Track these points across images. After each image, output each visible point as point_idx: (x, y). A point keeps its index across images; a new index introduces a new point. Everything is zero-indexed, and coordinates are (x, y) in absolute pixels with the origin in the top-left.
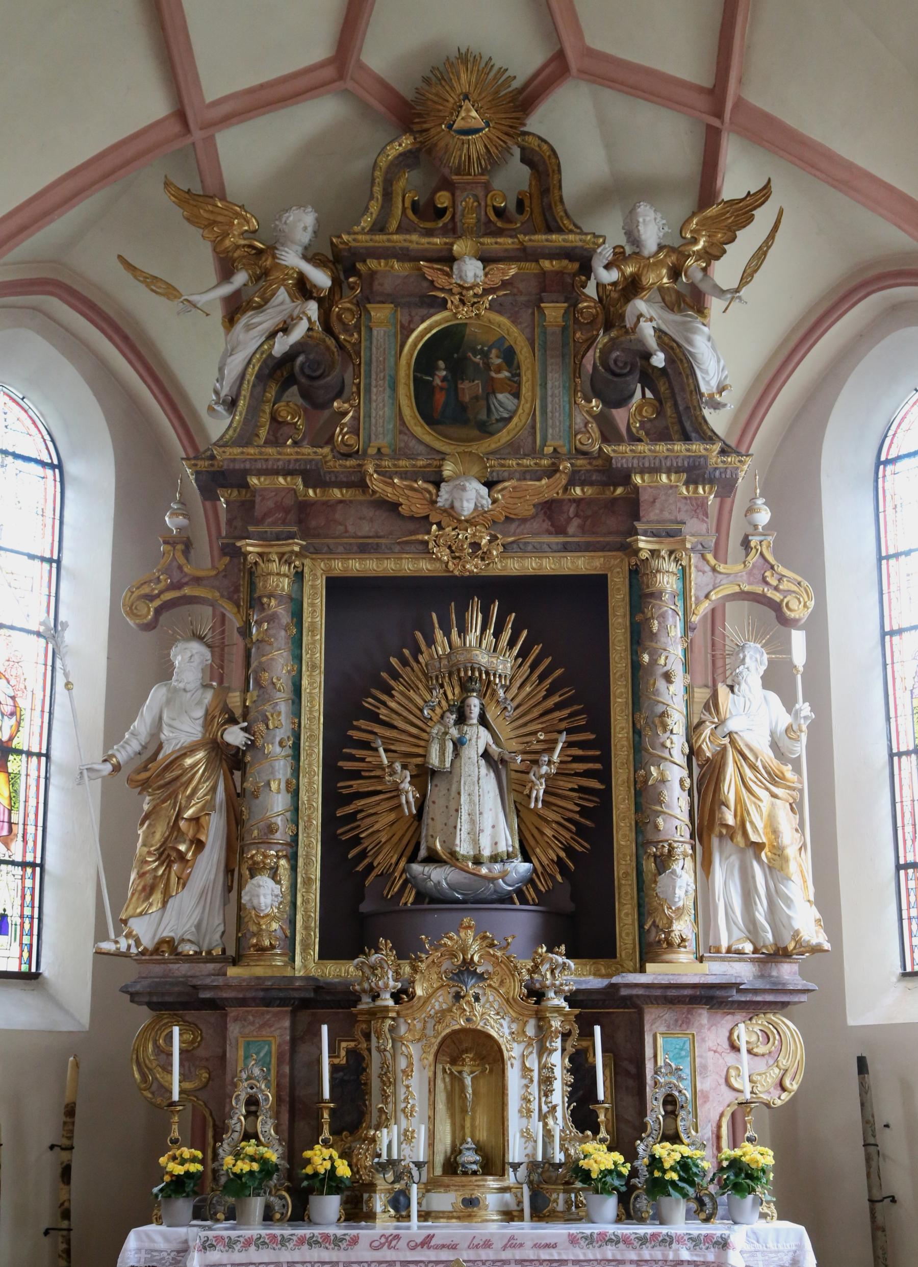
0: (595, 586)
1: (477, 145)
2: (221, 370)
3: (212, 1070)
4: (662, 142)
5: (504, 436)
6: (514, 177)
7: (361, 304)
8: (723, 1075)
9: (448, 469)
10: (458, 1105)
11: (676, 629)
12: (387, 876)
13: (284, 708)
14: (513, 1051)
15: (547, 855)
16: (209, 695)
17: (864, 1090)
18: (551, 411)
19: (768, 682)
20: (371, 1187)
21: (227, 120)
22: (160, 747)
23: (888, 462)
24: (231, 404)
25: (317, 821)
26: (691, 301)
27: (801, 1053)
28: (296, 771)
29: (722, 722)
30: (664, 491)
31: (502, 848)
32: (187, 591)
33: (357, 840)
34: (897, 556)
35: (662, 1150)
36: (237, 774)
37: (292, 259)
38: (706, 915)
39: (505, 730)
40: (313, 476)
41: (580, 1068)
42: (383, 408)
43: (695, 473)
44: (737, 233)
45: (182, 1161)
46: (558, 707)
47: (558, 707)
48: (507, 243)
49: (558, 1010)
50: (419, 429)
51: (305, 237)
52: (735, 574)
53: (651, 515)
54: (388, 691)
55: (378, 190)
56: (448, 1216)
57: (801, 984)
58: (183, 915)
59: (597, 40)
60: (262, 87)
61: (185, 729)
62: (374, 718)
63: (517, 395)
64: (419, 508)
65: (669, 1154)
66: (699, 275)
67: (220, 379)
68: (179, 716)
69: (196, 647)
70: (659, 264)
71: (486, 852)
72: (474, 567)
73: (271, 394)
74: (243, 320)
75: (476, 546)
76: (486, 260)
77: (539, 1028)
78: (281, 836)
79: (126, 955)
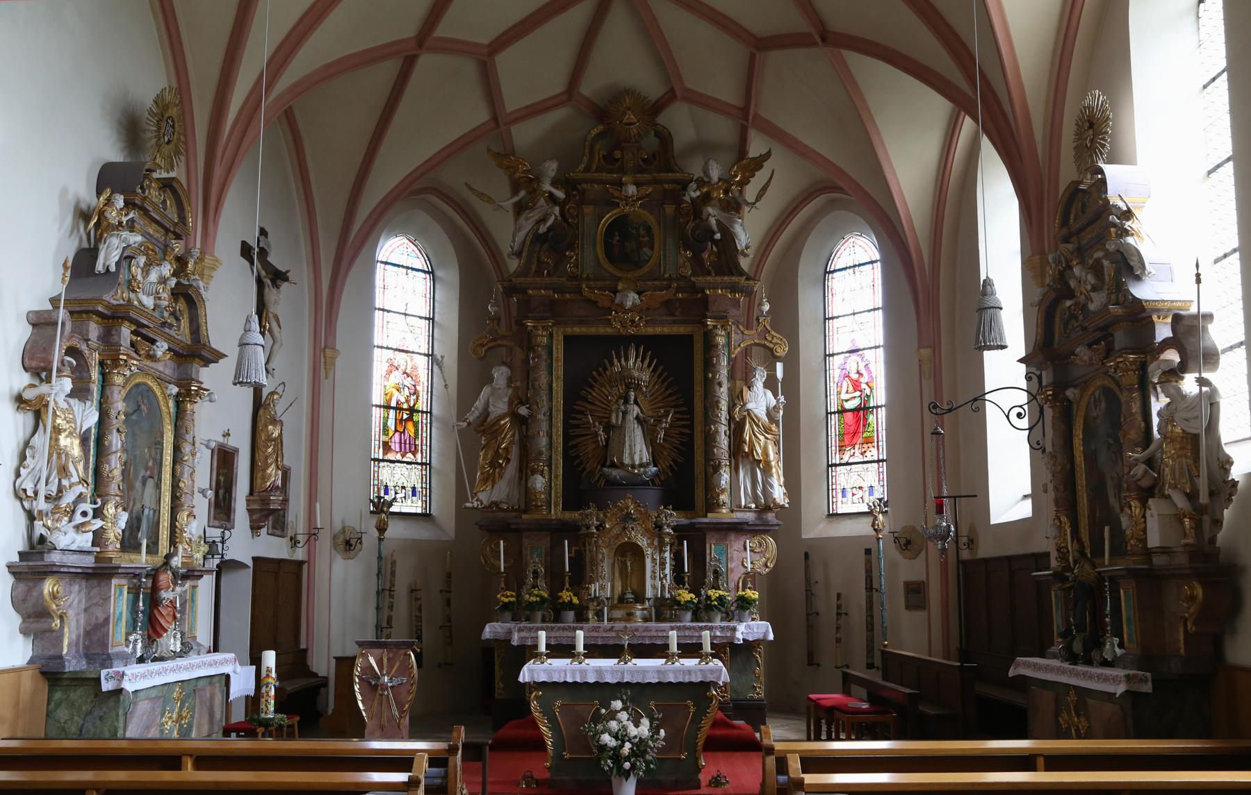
0: (688, 340)
1: (634, 130)
2: (514, 237)
3: (516, 557)
4: (722, 129)
5: (646, 269)
6: (651, 142)
8: (744, 559)
10: (624, 575)
11: (724, 362)
14: (649, 551)
16: (510, 391)
17: (807, 566)
18: (669, 257)
19: (766, 385)
20: (587, 608)
21: (516, 121)
22: (488, 414)
25: (560, 449)
26: (734, 206)
27: (775, 551)
28: (551, 426)
29: (745, 404)
31: (644, 460)
32: (499, 342)
33: (578, 456)
34: (833, 318)
35: (710, 592)
38: (735, 491)
41: (678, 558)
42: (589, 255)
43: (734, 288)
45: (507, 597)
46: (670, 395)
47: (670, 395)
48: (647, 177)
49: (669, 534)
50: (607, 265)
54: (592, 387)
55: (587, 151)
56: (620, 620)
57: (776, 521)
58: (500, 491)
61: (500, 407)
62: (586, 400)
63: (652, 249)
64: (607, 304)
65: (714, 594)
66: (737, 194)
67: (514, 241)
68: (496, 399)
69: (504, 369)
70: (719, 188)
72: (632, 331)
74: (524, 215)
75: (633, 321)
76: (638, 184)
78: (544, 457)
79: (477, 508)
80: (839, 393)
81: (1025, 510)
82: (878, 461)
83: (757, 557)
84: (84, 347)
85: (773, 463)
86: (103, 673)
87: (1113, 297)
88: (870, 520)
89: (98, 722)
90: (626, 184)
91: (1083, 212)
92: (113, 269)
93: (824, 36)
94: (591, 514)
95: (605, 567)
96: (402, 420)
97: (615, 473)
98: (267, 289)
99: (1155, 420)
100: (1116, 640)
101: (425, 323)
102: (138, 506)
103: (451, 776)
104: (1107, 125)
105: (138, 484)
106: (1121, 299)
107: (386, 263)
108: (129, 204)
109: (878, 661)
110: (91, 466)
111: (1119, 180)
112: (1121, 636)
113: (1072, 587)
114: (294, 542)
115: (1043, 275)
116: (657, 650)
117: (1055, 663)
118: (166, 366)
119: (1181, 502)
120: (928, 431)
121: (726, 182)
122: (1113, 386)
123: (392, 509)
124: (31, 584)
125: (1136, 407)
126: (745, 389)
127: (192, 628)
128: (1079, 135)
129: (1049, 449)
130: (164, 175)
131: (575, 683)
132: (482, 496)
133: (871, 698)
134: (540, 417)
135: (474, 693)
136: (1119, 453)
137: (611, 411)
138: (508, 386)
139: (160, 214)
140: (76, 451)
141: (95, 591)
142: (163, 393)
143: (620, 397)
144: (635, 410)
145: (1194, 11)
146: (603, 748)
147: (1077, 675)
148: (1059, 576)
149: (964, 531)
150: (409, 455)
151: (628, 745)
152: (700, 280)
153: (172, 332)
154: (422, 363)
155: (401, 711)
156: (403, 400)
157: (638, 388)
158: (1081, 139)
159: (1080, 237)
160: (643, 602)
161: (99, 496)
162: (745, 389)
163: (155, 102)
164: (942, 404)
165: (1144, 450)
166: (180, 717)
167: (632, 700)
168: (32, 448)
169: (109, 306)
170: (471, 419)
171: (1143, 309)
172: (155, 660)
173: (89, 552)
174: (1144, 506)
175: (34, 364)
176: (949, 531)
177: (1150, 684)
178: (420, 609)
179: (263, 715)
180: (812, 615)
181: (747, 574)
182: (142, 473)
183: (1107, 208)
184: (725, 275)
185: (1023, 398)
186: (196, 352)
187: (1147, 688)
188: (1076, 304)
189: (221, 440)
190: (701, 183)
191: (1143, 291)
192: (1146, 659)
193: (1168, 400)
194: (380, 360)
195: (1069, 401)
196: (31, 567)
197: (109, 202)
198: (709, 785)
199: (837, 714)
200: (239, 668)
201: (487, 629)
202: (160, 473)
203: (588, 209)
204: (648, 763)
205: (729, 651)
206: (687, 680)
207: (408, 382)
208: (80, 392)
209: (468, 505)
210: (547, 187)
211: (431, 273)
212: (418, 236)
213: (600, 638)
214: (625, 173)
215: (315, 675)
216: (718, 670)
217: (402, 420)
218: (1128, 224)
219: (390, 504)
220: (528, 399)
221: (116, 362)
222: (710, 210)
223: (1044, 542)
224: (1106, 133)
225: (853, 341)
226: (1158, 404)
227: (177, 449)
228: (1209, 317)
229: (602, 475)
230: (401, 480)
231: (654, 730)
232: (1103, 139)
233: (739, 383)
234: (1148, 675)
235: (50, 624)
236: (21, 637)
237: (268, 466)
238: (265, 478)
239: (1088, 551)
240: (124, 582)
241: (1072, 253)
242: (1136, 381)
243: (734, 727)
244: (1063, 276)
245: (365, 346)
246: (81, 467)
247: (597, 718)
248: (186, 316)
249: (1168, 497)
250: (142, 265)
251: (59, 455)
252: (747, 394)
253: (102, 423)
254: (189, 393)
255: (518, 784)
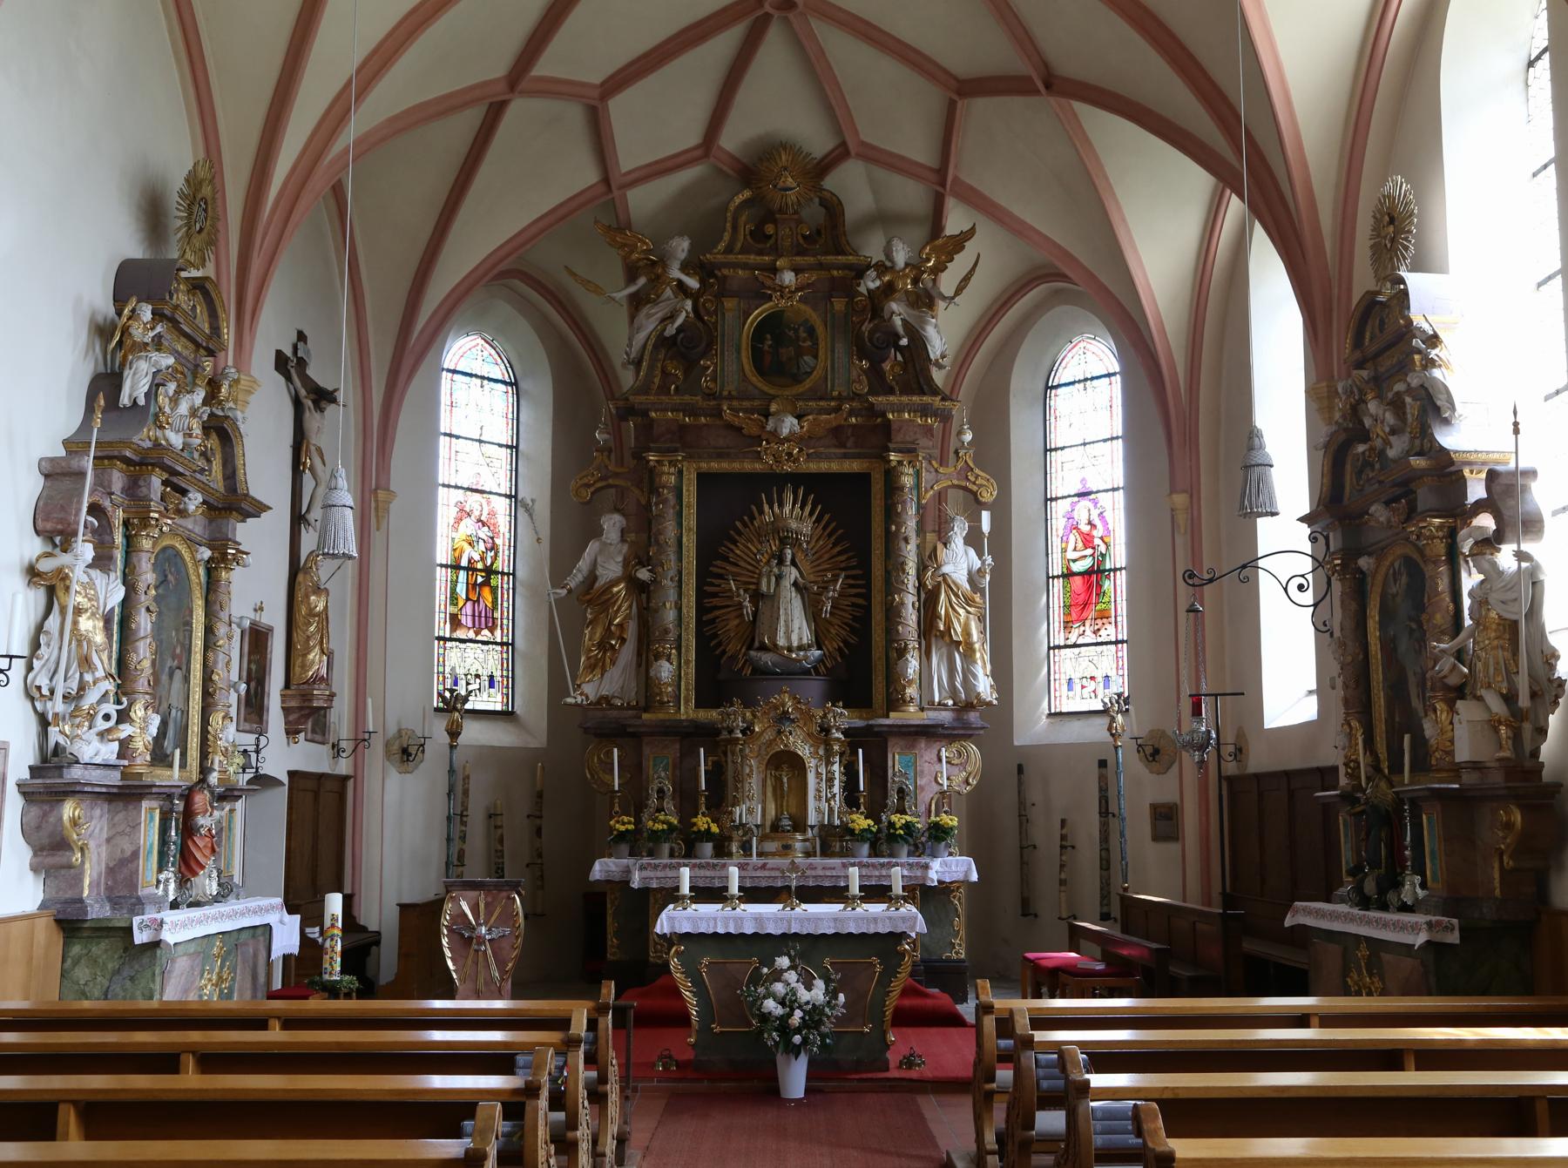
0: (863, 479)
1: (792, 196)
2: (630, 339)
4: (910, 195)
5: (808, 384)
6: (813, 213)
7: (720, 295)
8: (938, 776)
9: (773, 407)
10: (779, 794)
11: (912, 511)
12: (734, 658)
13: (673, 557)
14: (811, 763)
15: (832, 645)
16: (625, 548)
18: (834, 364)
20: (730, 839)
23: (1053, 387)
24: (637, 364)
25: (693, 625)
26: (925, 300)
29: (939, 567)
30: (901, 411)
31: (805, 641)
32: (610, 481)
33: (715, 635)
34: (1056, 449)
35: (894, 818)
36: (644, 596)
37: (675, 273)
38: (927, 681)
39: (806, 566)
40: (692, 411)
42: (732, 365)
43: (925, 411)
44: (298, 917)
45: (624, 824)
46: (840, 553)
47: (840, 553)
49: (838, 739)
50: (755, 379)
51: (683, 256)
52: (948, 476)
53: (898, 438)
54: (735, 542)
55: (728, 225)
56: (773, 854)
57: (980, 723)
59: (867, 136)
60: (657, 162)
61: (611, 569)
62: (726, 559)
63: (816, 357)
64: (755, 431)
66: (930, 285)
68: (606, 557)
69: (617, 518)
70: (906, 276)
71: (795, 644)
72: (788, 468)
73: (661, 356)
74: (645, 311)
75: (790, 454)
76: (797, 271)
77: (826, 750)
78: (672, 637)
80: (1064, 551)
81: (1307, 710)
82: (1117, 642)
83: (956, 770)
84: (107, 503)
85: (977, 646)
86: (136, 920)
87: (1417, 442)
88: (1105, 721)
89: (128, 983)
90: (781, 270)
91: (1381, 331)
92: (142, 401)
93: (1052, 83)
94: (735, 713)
95: (754, 784)
96: (475, 584)
97: (767, 658)
98: (307, 414)
99: (1466, 602)
100: (1418, 879)
101: (505, 452)
102: (165, 705)
103: (602, 1042)
104: (1411, 223)
105: (164, 678)
106: (1427, 445)
107: (454, 372)
108: (158, 315)
109: (1116, 911)
110: (114, 656)
111: (1429, 297)
112: (1423, 875)
113: (1363, 812)
114: (337, 750)
115: (1331, 408)
116: (836, 894)
117: (1342, 908)
118: (195, 526)
119: (1497, 706)
120: (1183, 606)
121: (916, 268)
122: (1416, 556)
123: (468, 706)
124: (46, 807)
125: (1443, 585)
126: (940, 546)
127: (229, 865)
128: (1377, 230)
129: (1337, 634)
130: (195, 273)
131: (728, 934)
132: (588, 689)
133: (1106, 957)
134: (666, 582)
135: (589, 943)
136: (1421, 641)
137: (760, 574)
138: (623, 540)
139: (190, 326)
140: (99, 638)
141: (121, 816)
142: (193, 558)
143: (773, 556)
144: (793, 574)
145: (1522, 77)
146: (765, 1017)
147: (1369, 922)
148: (1348, 798)
149: (1229, 737)
150: (486, 632)
151: (798, 1014)
152: (879, 400)
153: (203, 478)
154: (502, 506)
155: (502, 971)
156: (477, 557)
157: (796, 543)
158: (1378, 236)
159: (1375, 362)
160: (804, 831)
161: (125, 694)
162: (940, 546)
163: (187, 180)
164: (1201, 571)
165: (1453, 638)
166: (220, 977)
167: (803, 955)
168: (47, 633)
169: (138, 450)
170: (572, 585)
171: (1452, 463)
172: (190, 905)
173: (114, 767)
174: (1452, 709)
175: (49, 526)
176: (1210, 738)
177: (1457, 933)
178: (501, 841)
179: (326, 977)
180: (1026, 848)
181: (943, 793)
182: (169, 663)
183: (1409, 329)
184: (913, 393)
185: (1306, 565)
186: (233, 503)
187: (1454, 938)
188: (1372, 449)
189: (252, 615)
190: (882, 268)
191: (1448, 439)
192: (1451, 904)
193: (1482, 577)
194: (447, 505)
195: (1362, 572)
196: (46, 786)
197: (134, 314)
198: (900, 1067)
199: (1063, 977)
200: (287, 917)
201: (597, 866)
202: (189, 662)
203: (729, 304)
204: (823, 1036)
205: (928, 896)
206: (872, 931)
207: (484, 533)
208: (102, 561)
209: (569, 700)
210: (675, 273)
211: (514, 384)
212: (496, 335)
213: (764, 879)
214: (781, 256)
215: (364, 929)
216: (911, 920)
217: (475, 584)
218: (1433, 353)
219: (466, 700)
220: (649, 558)
221: (145, 522)
222: (894, 306)
223: (1329, 755)
224: (1410, 232)
225: (1083, 480)
226: (1470, 580)
227: (209, 630)
228: (1531, 474)
229: (748, 661)
230: (473, 664)
231: (832, 994)
232: (1406, 239)
233: (930, 537)
234: (1455, 921)
235: (70, 858)
236: (30, 875)
237: (308, 650)
238: (304, 667)
239: (1385, 766)
240: (155, 804)
241: (1367, 382)
242: (1443, 551)
243: (927, 996)
244: (1355, 410)
245: (428, 484)
246: (105, 657)
247: (756, 979)
248: (218, 456)
249: (1480, 699)
250: (171, 393)
251: (79, 643)
252: (942, 553)
253: (126, 604)
254: (224, 557)
255: (654, 1065)
